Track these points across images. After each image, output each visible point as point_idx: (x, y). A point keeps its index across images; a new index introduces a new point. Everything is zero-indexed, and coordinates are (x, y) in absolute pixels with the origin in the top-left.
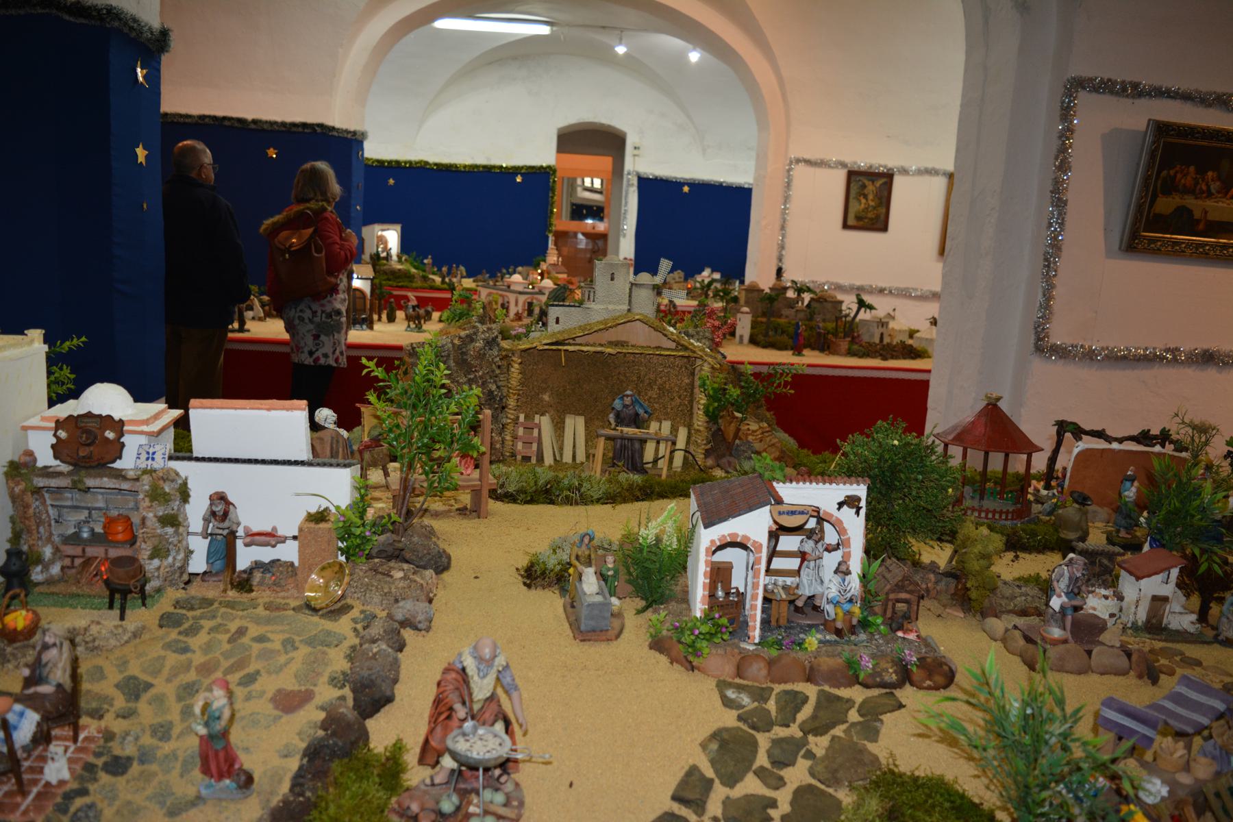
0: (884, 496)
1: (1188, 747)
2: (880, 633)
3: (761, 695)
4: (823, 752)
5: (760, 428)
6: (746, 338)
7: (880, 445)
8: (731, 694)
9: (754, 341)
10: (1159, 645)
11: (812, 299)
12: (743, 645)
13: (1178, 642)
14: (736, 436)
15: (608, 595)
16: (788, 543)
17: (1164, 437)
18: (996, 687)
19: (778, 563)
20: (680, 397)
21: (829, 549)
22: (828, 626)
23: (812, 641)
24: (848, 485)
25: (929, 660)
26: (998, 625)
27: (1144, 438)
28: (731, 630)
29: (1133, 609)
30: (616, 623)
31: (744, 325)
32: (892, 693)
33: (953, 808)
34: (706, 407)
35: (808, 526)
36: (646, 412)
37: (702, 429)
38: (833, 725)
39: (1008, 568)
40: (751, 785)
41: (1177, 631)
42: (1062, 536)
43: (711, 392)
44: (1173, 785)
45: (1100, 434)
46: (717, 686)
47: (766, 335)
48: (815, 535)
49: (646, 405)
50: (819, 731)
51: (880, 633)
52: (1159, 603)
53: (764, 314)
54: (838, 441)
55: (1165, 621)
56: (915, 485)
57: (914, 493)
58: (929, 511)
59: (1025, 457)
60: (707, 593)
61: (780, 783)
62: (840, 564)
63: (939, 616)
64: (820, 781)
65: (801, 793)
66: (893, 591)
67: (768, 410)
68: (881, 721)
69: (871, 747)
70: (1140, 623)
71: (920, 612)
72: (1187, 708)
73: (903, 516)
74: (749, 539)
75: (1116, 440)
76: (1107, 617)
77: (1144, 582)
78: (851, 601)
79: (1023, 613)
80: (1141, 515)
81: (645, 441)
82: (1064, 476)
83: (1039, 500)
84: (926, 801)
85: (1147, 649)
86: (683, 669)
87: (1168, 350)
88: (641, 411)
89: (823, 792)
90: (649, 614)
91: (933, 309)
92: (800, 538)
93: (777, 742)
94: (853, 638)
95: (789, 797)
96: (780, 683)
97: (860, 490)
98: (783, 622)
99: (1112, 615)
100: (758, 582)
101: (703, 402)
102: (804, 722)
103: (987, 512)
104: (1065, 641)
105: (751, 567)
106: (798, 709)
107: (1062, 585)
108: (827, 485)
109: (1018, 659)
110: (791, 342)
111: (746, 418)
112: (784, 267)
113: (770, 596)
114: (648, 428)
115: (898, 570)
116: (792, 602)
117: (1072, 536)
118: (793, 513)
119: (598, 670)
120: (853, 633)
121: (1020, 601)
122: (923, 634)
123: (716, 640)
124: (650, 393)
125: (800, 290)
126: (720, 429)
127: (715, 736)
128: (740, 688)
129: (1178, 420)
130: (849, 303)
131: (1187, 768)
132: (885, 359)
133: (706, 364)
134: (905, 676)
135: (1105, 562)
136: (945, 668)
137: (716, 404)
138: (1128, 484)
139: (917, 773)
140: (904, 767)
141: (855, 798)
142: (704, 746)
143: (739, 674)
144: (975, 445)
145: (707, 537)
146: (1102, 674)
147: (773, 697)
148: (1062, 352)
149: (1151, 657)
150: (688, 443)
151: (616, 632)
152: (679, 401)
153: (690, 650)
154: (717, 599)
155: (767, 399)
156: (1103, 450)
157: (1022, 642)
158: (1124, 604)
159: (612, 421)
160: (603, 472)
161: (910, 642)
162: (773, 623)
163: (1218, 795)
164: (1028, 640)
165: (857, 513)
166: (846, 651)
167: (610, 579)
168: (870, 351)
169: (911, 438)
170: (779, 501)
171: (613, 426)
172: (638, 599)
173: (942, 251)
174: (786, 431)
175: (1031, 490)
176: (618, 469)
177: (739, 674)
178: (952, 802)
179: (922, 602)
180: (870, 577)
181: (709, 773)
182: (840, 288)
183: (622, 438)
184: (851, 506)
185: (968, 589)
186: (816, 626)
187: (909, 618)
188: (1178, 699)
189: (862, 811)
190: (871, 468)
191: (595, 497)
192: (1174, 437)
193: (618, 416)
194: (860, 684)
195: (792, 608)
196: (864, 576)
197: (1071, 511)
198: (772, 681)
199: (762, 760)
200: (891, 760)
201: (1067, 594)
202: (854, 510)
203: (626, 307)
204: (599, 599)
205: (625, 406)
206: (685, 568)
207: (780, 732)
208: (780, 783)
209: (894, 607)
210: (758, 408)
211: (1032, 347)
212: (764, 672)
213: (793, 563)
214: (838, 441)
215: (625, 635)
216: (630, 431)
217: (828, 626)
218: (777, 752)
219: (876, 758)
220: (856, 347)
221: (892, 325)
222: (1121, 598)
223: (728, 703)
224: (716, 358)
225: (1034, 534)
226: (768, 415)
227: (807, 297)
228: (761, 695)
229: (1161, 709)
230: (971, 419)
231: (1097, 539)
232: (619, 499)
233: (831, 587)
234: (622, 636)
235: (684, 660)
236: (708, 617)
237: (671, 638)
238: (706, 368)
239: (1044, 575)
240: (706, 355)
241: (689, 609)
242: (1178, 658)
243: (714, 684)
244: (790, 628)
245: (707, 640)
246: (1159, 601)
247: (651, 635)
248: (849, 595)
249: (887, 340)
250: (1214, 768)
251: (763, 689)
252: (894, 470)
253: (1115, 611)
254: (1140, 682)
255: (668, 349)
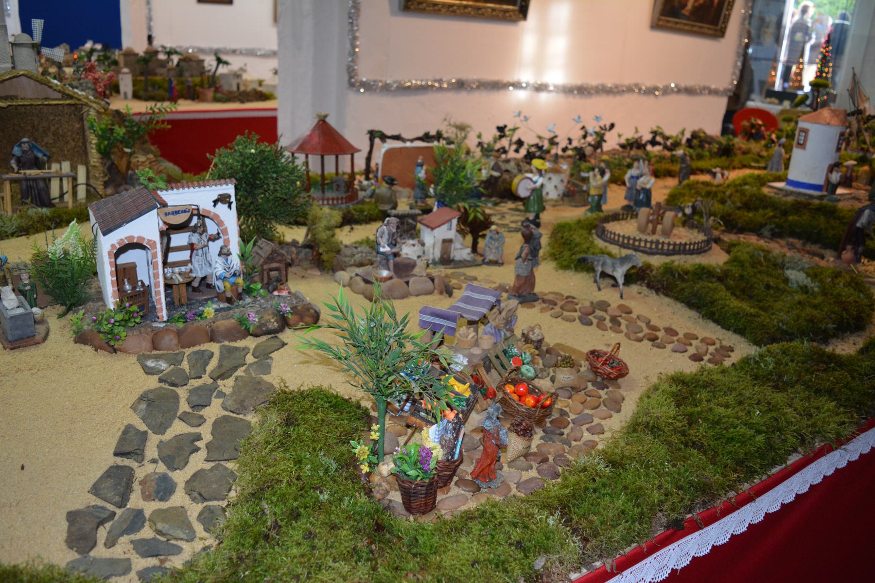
0: (249, 193)
1: (476, 331)
2: (261, 296)
3: (175, 361)
4: (231, 390)
5: (148, 159)
6: (130, 94)
7: (241, 154)
8: (150, 363)
9: (136, 96)
10: (450, 271)
11: (180, 60)
12: (155, 325)
13: (461, 267)
14: (128, 167)
15: (28, 307)
16: (179, 239)
17: (439, 136)
18: (347, 312)
19: (173, 257)
20: (74, 140)
21: (213, 238)
22: (221, 297)
23: (209, 310)
24: (219, 186)
25: (299, 308)
26: (344, 275)
27: (426, 137)
28: (141, 314)
29: (431, 251)
30: (41, 329)
31: (126, 83)
32: (276, 337)
33: (331, 406)
34: (98, 146)
35: (192, 224)
36: (45, 155)
37: (97, 164)
38: (236, 368)
39: (347, 237)
40: (178, 428)
41: (460, 261)
42: (381, 208)
43: (100, 132)
44: (470, 357)
45: (397, 138)
46: (138, 360)
47: (146, 90)
48: (201, 229)
49: (44, 149)
50: (223, 376)
51: (261, 296)
52: (447, 244)
53: (142, 74)
54: (208, 155)
55: (452, 256)
56: (271, 182)
57: (272, 188)
58: (285, 200)
59: (349, 156)
60: (116, 288)
61: (202, 420)
62: (221, 248)
63: (303, 277)
64: (231, 411)
65: (216, 424)
66: (265, 263)
67: (153, 144)
68: (271, 358)
69: (267, 378)
70: (437, 259)
71: (289, 277)
72: (471, 305)
73: (266, 207)
74: (143, 239)
75: (409, 140)
76: (415, 258)
77: (436, 231)
78: (234, 275)
79: (361, 265)
80: (429, 186)
81: (50, 180)
82: (377, 170)
83: (363, 189)
84: (312, 406)
85: (443, 275)
86: (107, 353)
87: (435, 81)
88: (40, 155)
89: (235, 419)
90: (70, 316)
91: (273, 63)
92: (189, 234)
93: (192, 392)
94: (241, 302)
95: (210, 429)
96: (189, 347)
97: (229, 189)
98: (184, 300)
99: (419, 257)
100: (158, 273)
101: (94, 142)
102: (212, 372)
103: (328, 199)
104: (391, 278)
105: (152, 264)
106: (206, 364)
107: (383, 241)
108: (202, 188)
109: (361, 296)
110: (167, 95)
111: (134, 153)
112: (154, 35)
113: (169, 282)
114: (49, 168)
115: (266, 247)
116: (189, 284)
117: (386, 207)
118: (177, 212)
119: (30, 369)
120: (240, 299)
121: (358, 257)
122: (293, 291)
123: (131, 325)
124: (46, 140)
125: (170, 53)
126: (113, 164)
127: (142, 398)
128: (157, 358)
129: (446, 123)
130: (210, 62)
131: (476, 344)
132: (242, 102)
133: (91, 110)
134: (284, 323)
135: (410, 221)
136: (312, 311)
137: (106, 143)
138: (419, 168)
139: (302, 389)
140: (293, 386)
141: (260, 416)
142: (134, 408)
143: (155, 347)
144: (313, 151)
145: (107, 243)
146: (417, 296)
147: (185, 358)
148: (368, 86)
149: (447, 280)
150: (88, 178)
151: (43, 335)
152: (73, 144)
153: (109, 336)
154: (126, 292)
155: (150, 135)
156: (401, 149)
157: (362, 284)
158: (426, 248)
159: (14, 166)
160: (14, 211)
161: (285, 297)
162: (177, 303)
163: (497, 357)
164: (367, 282)
165: (230, 207)
166: (237, 313)
167: (28, 293)
168: (230, 97)
169: (264, 146)
170: (164, 205)
171: (16, 170)
172: (58, 306)
173: (276, 19)
174: (170, 160)
175: (356, 182)
176: (27, 206)
177: (155, 347)
178: (330, 402)
179: (290, 269)
180: (247, 255)
181: (143, 427)
182: (202, 51)
183: (27, 179)
184: (223, 202)
185: (321, 254)
186: (211, 299)
187: (281, 281)
188: (467, 300)
189: (266, 425)
190: (237, 173)
191: (10, 232)
192: (445, 135)
193: (19, 161)
194: (251, 335)
195: (190, 289)
196: (242, 255)
197: (383, 189)
198: (183, 347)
199: (184, 407)
200: (282, 384)
201: (388, 245)
202: (227, 205)
203: (10, 65)
204: (20, 311)
205: (24, 152)
206: (96, 274)
207: (195, 383)
208: (202, 420)
209: (269, 275)
210: (144, 143)
211: (346, 84)
212: (175, 341)
213: (185, 255)
214: (208, 155)
215: (52, 336)
216: (33, 173)
217: (221, 297)
218: (194, 399)
219: (272, 385)
220: (219, 95)
221: (245, 76)
222: (423, 245)
223: (149, 371)
224: (99, 104)
225: (362, 211)
226: (153, 148)
227: (175, 59)
228: (175, 361)
229: (457, 308)
230: (308, 133)
231: (403, 207)
232: (32, 230)
233: (219, 267)
234: (49, 338)
235: (106, 345)
236: (120, 307)
237: (92, 330)
238: (92, 113)
239: (372, 238)
240: (91, 101)
241: (105, 305)
242: (462, 278)
243: (135, 359)
244: (191, 304)
245: (123, 326)
246: (447, 242)
247: (74, 332)
248: (232, 271)
249: (242, 88)
250: (493, 340)
251: (176, 354)
252: (254, 172)
253: (420, 253)
254: (441, 297)
255: (56, 99)
